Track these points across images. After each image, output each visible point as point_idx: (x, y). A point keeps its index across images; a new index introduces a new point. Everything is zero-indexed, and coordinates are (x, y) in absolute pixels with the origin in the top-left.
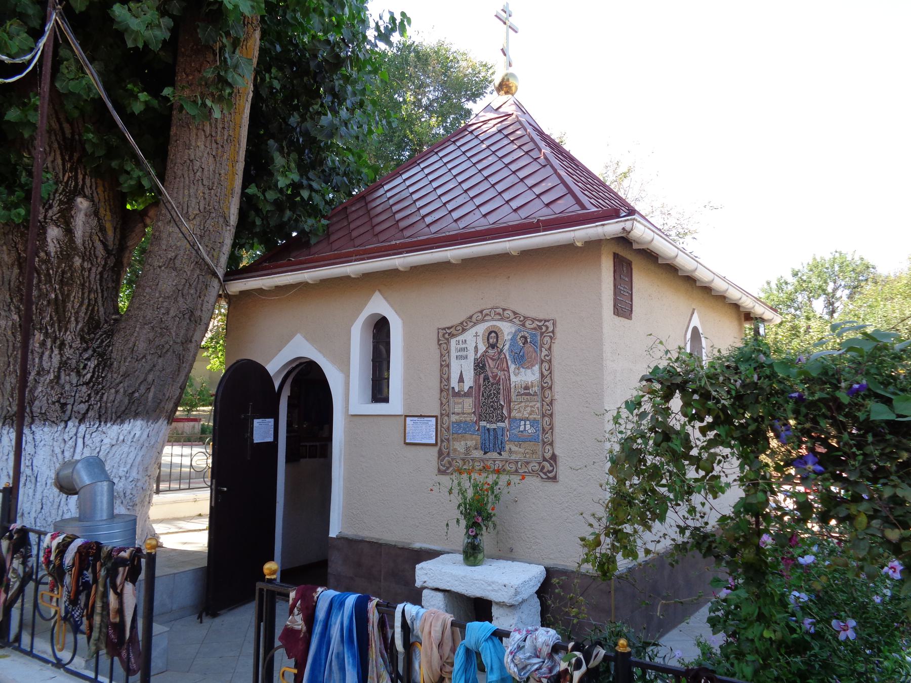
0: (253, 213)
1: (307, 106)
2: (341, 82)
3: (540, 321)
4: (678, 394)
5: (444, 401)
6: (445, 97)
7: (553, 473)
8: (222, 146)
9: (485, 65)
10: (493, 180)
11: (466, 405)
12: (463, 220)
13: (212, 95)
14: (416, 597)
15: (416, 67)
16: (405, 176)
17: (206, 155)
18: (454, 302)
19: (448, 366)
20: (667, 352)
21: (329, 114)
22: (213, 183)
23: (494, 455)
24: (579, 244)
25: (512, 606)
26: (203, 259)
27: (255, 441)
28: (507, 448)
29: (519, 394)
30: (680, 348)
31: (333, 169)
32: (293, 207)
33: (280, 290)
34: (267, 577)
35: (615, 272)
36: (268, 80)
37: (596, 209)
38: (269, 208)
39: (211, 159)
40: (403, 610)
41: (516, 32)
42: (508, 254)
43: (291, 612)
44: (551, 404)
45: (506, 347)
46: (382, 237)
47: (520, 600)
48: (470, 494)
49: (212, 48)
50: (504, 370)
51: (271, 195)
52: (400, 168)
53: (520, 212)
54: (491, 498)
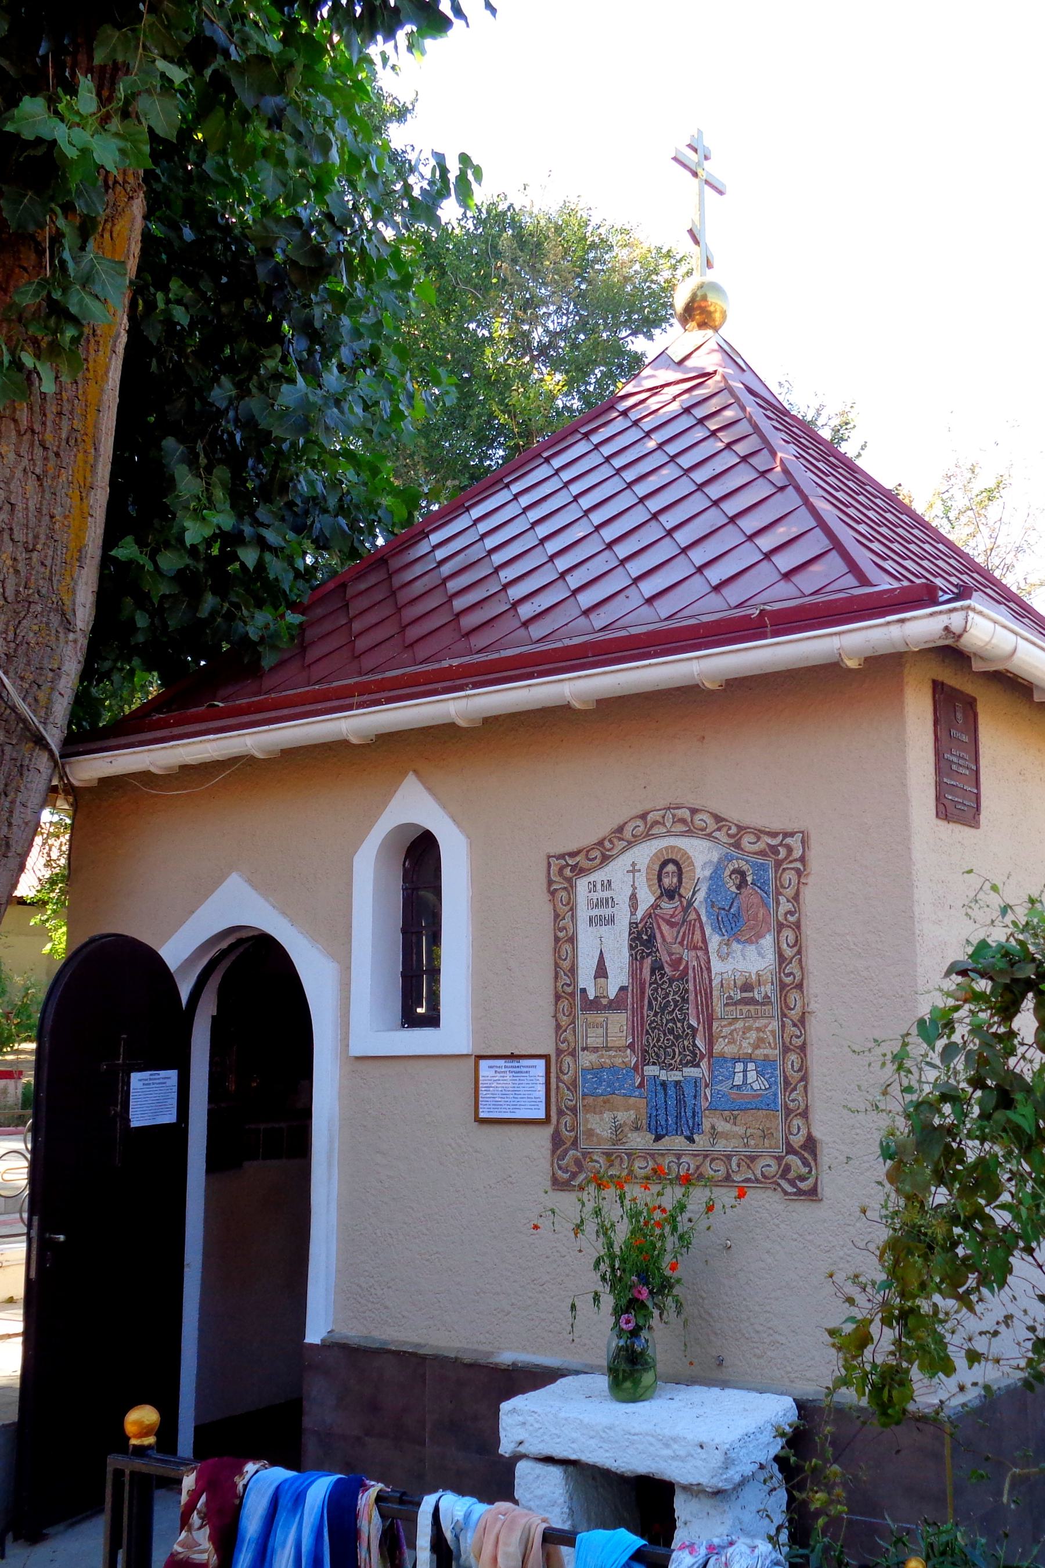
0: (129, 600)
1: (253, 362)
2: (328, 308)
3: (773, 835)
4: (1029, 1002)
5: (564, 1021)
6: (582, 326)
7: (810, 1182)
8: (57, 455)
9: (669, 255)
10: (669, 520)
11: (613, 1029)
12: (602, 610)
13: (35, 342)
14: (495, 1481)
15: (514, 261)
16: (476, 513)
17: (19, 474)
18: (580, 797)
19: (572, 940)
20: (1005, 909)
21: (299, 379)
22: (36, 537)
23: (677, 1142)
24: (852, 664)
25: (718, 1493)
26: (14, 709)
27: (133, 1124)
28: (706, 1125)
29: (731, 1002)
30: (1032, 901)
31: (315, 502)
32: (222, 585)
33: (189, 773)
34: (134, 1442)
35: (936, 722)
36: (161, 305)
37: (896, 585)
38: (164, 589)
39: (32, 484)
40: (437, 1509)
41: (721, 193)
42: (698, 686)
43: (185, 1522)
44: (802, 1022)
45: (701, 896)
46: (423, 651)
47: (737, 1478)
48: (622, 1233)
49: (32, 237)
50: (695, 948)
51: (170, 562)
52: (482, 483)
53: (726, 591)
54: (671, 1242)
